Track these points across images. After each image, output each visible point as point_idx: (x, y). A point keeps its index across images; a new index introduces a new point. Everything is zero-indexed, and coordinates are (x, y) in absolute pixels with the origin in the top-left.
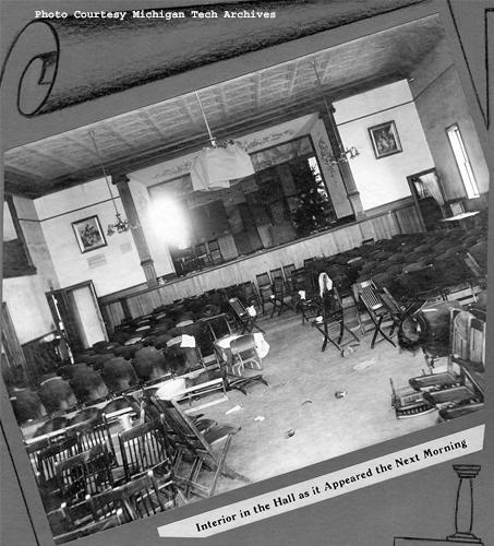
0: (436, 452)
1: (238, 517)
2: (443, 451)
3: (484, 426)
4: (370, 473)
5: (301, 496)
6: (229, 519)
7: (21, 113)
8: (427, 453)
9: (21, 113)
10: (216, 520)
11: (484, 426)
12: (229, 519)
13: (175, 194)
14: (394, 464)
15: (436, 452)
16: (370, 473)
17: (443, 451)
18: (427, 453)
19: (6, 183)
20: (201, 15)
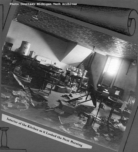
0: (74, 143)
1: (18, 123)
2: (76, 144)
3: (2, 114)
4: (55, 136)
5: (40, 131)
6: (15, 122)
7: (134, 18)
8: (72, 141)
9: (135, 20)
10: (53, 136)
11: (2, 114)
12: (15, 122)
13: (115, 75)
14: (62, 138)
15: (74, 143)
16: (55, 136)
17: (76, 144)
18: (72, 141)
19: (2, 73)
20: (56, 4)
